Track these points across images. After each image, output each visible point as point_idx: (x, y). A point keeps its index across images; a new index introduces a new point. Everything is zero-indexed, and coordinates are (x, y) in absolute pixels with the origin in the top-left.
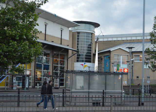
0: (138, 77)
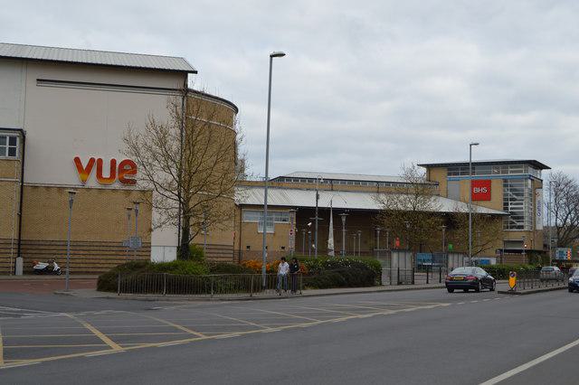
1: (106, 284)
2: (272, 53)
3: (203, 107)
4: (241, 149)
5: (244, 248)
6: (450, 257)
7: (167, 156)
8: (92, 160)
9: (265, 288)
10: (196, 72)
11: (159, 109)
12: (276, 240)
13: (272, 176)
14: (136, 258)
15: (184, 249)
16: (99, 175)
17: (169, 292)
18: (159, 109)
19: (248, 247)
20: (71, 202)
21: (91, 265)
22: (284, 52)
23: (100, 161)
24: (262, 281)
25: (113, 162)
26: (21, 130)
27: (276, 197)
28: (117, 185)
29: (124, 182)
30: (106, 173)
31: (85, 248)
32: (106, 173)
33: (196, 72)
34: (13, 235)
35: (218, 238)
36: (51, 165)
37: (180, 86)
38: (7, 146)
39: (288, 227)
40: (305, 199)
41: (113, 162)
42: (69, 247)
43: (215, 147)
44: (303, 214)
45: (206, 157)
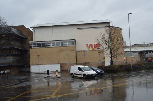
0: (129, 61)
2: (129, 13)
3: (113, 29)
4: (124, 36)
5: (128, 61)
7: (105, 41)
8: (90, 44)
9: (132, 70)
10: (111, 22)
11: (103, 31)
12: (134, 59)
13: (132, 44)
16: (92, 47)
17: (108, 73)
18: (103, 31)
19: (129, 61)
20: (85, 53)
21: (64, 69)
22: (131, 13)
23: (92, 44)
24: (132, 69)
26: (75, 39)
27: (133, 49)
28: (96, 49)
29: (97, 48)
30: (94, 47)
31: (91, 64)
32: (94, 47)
33: (111, 22)
34: (76, 62)
35: (121, 60)
36: (82, 47)
37: (108, 26)
38: (72, 43)
39: (136, 54)
40: (142, 49)
41: (95, 44)
43: (116, 38)
44: (141, 52)
45: (115, 40)
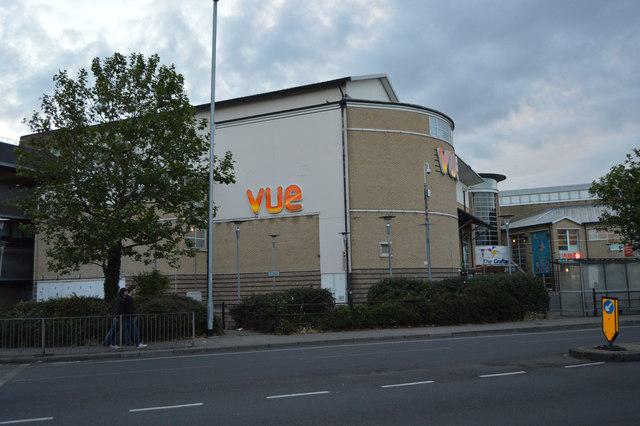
1: (348, 79)
6: (591, 239)
8: (261, 190)
14: (306, 284)
15: (350, 297)
16: (268, 206)
25: (280, 189)
30: (274, 203)
32: (274, 203)
37: (339, 98)
41: (280, 189)
42: (239, 289)
